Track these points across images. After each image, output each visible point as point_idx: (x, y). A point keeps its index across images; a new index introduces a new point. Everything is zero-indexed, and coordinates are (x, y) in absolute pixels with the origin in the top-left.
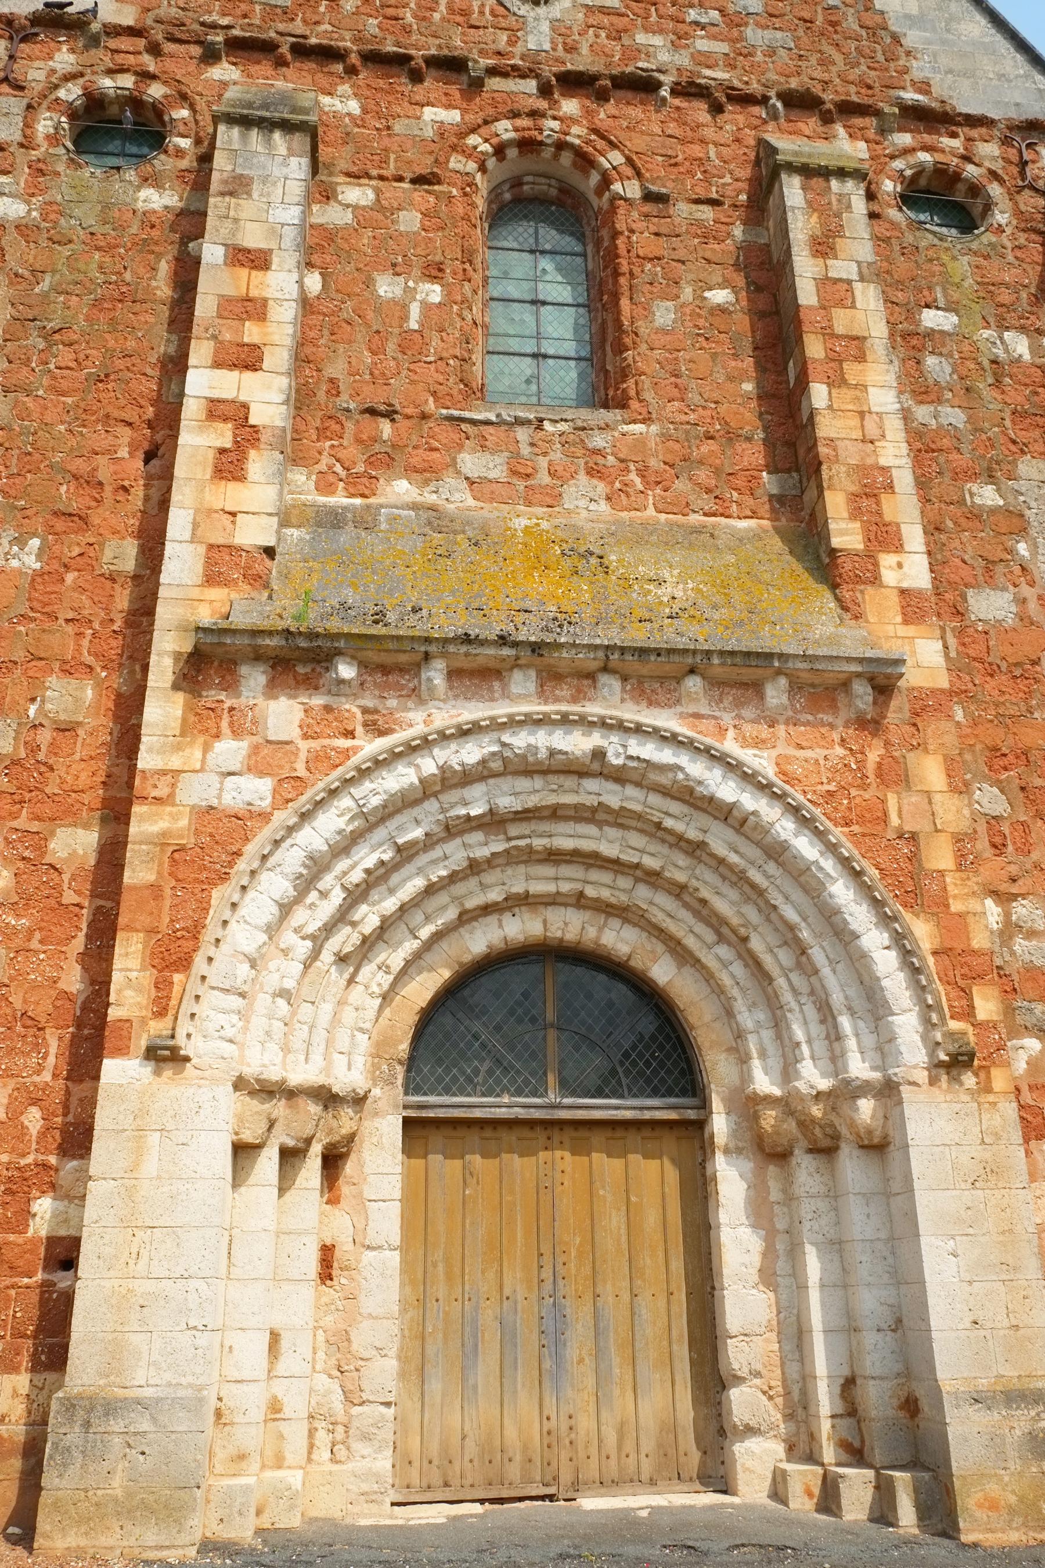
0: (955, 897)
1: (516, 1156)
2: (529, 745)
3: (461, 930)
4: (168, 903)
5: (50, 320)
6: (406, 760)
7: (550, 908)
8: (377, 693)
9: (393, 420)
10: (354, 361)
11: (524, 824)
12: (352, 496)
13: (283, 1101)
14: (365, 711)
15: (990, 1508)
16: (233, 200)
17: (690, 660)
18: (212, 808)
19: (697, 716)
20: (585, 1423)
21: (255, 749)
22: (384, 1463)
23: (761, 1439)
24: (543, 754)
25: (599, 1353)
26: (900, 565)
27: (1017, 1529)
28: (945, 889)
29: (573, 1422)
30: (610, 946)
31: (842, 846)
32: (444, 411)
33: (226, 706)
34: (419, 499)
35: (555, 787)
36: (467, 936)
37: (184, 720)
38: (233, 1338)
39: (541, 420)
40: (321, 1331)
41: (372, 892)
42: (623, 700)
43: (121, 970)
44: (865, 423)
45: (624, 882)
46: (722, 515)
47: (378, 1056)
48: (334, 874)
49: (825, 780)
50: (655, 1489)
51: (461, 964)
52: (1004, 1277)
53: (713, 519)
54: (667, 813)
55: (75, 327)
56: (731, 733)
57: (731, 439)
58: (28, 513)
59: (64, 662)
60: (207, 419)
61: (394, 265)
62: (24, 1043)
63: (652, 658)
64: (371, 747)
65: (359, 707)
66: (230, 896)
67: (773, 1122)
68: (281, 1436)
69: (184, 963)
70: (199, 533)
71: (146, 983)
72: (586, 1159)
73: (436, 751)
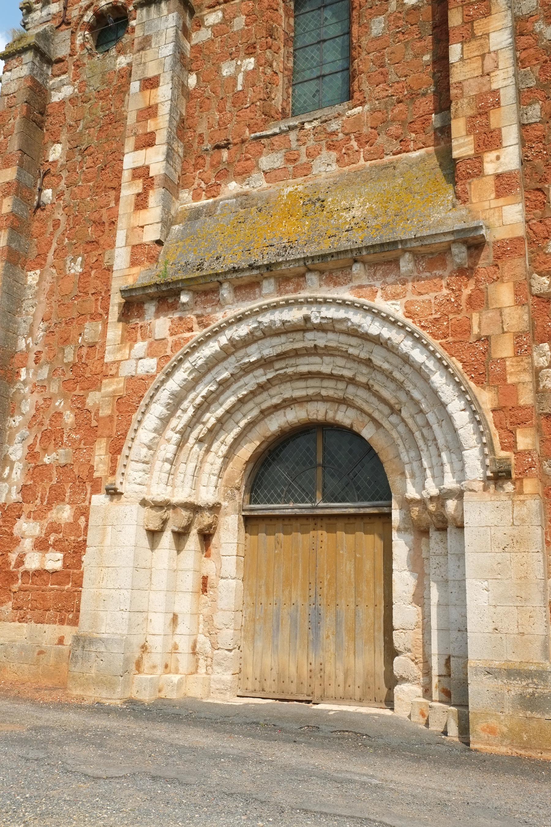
0: (511, 374)
1: (299, 534)
2: (271, 321)
3: (266, 420)
4: (115, 423)
5: (83, 145)
6: (214, 339)
7: (309, 403)
8: (202, 306)
9: (228, 149)
10: (210, 120)
11: (283, 362)
12: (209, 198)
13: (171, 510)
14: (198, 316)
15: (490, 732)
16: (144, 52)
17: (350, 256)
18: (133, 376)
19: (360, 287)
20: (329, 668)
21: (151, 345)
22: (227, 677)
23: (410, 684)
24: (278, 324)
25: (337, 634)
26: (498, 158)
27: (506, 746)
28: (505, 370)
29: (322, 667)
30: (340, 421)
31: (437, 352)
32: (253, 135)
33: (139, 326)
34: (241, 190)
35: (291, 340)
36: (268, 422)
37: (122, 335)
38: (151, 616)
39: (303, 123)
40: (201, 616)
41: (212, 406)
42: (320, 286)
43: (98, 455)
44: (485, 62)
45: (341, 385)
46: (404, 151)
47: (227, 486)
48: (188, 400)
49: (433, 312)
50: (361, 704)
51: (265, 437)
52: (518, 604)
53: (399, 155)
54: (350, 345)
55: (93, 145)
56: (379, 294)
57: (413, 98)
58: (77, 245)
59: (92, 314)
60: (132, 180)
61: (231, 54)
62: (79, 489)
63: (329, 259)
64: (198, 333)
65: (195, 315)
66: (137, 418)
67: (417, 513)
68: (177, 660)
69: (119, 451)
70: (128, 241)
71: (107, 460)
72: (334, 534)
73: (227, 332)
